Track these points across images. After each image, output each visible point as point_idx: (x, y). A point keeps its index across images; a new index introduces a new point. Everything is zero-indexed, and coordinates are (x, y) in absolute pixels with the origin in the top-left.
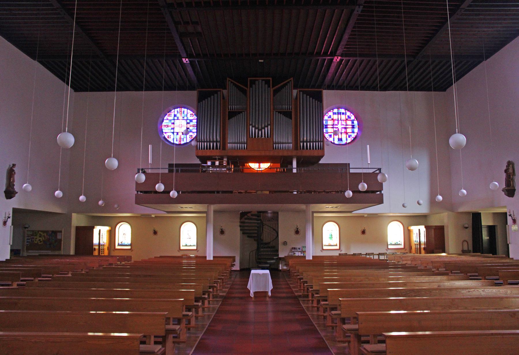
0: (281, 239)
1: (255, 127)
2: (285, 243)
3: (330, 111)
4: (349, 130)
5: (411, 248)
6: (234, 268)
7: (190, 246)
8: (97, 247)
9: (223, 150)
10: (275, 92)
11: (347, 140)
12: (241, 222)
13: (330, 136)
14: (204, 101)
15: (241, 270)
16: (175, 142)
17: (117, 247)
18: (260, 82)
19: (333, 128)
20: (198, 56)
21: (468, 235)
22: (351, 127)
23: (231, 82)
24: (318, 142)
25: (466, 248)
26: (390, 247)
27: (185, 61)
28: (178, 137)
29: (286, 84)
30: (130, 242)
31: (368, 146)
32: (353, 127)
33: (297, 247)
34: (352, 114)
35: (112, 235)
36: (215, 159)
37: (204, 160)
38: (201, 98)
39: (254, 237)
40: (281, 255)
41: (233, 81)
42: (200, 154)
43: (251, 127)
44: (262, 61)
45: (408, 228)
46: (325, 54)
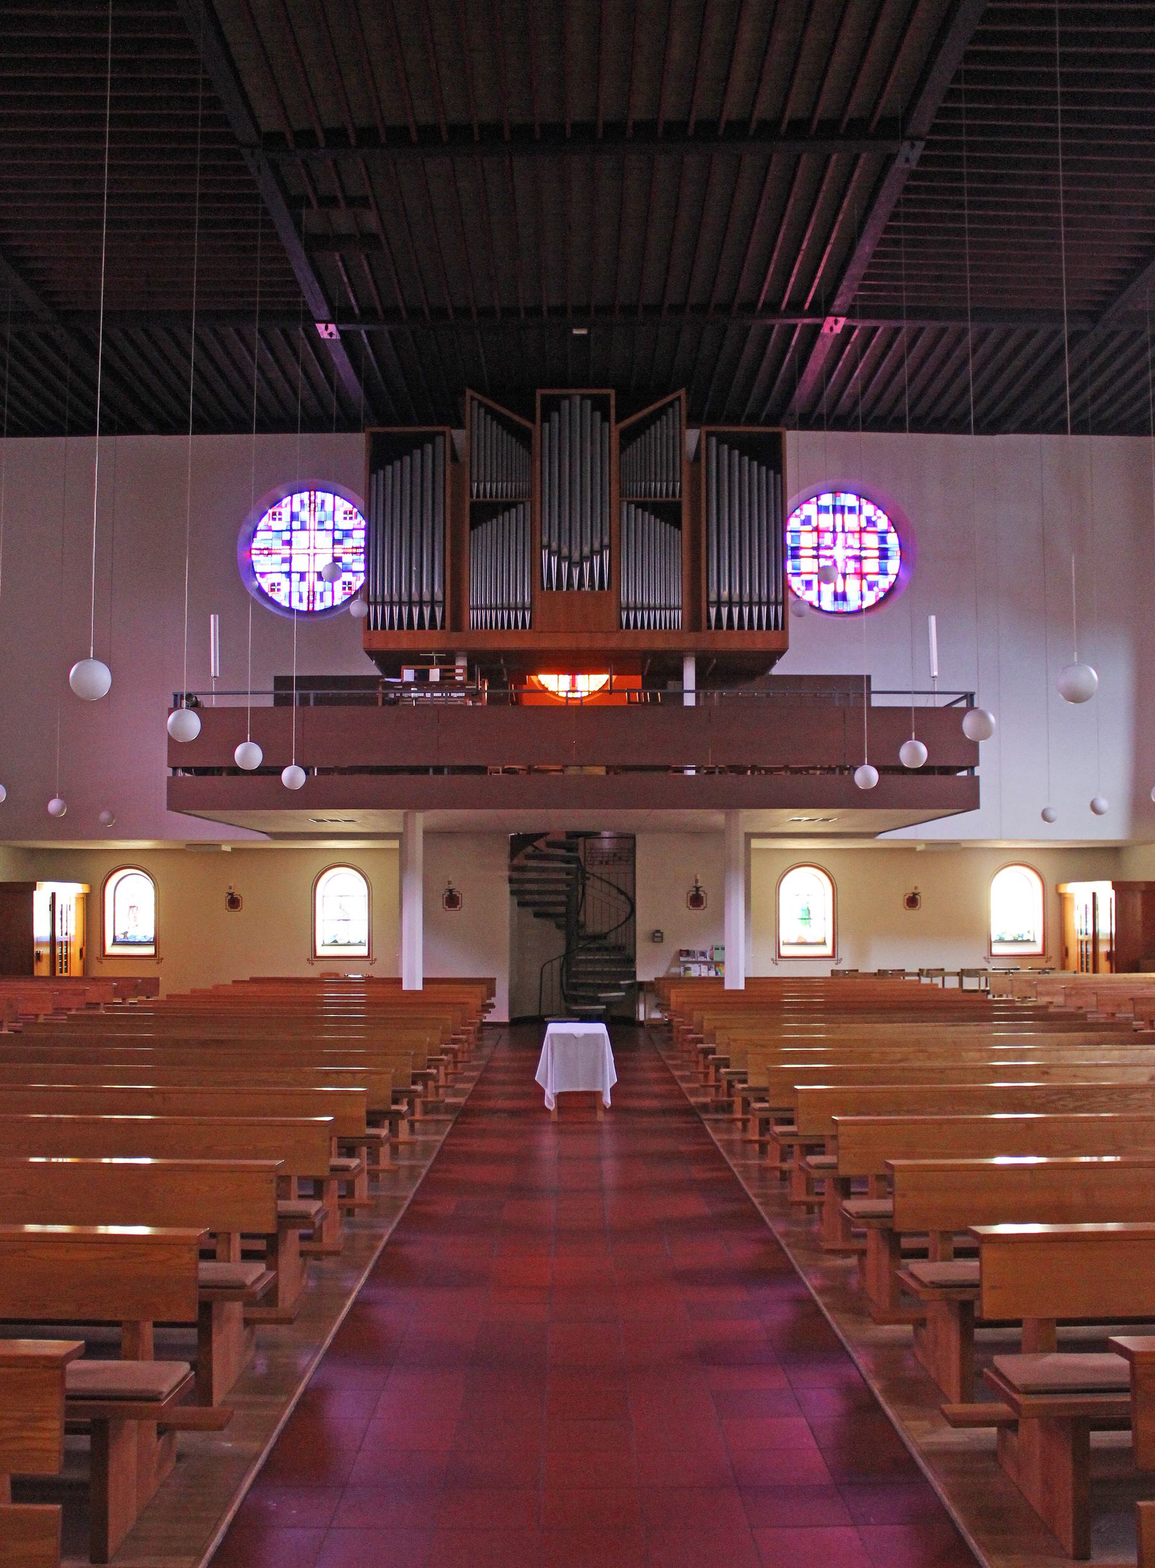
0: (644, 923)
1: (559, 552)
2: (657, 936)
3: (807, 502)
4: (871, 566)
6: (489, 1018)
7: (349, 944)
8: (45, 951)
10: (628, 437)
11: (862, 598)
12: (513, 868)
13: (808, 584)
14: (407, 459)
16: (296, 605)
17: (111, 950)
18: (577, 403)
19: (817, 557)
20: (368, 314)
22: (877, 553)
23: (480, 404)
26: (997, 949)
27: (327, 331)
28: (304, 587)
29: (662, 411)
30: (150, 935)
31: (933, 619)
32: (884, 554)
33: (697, 948)
34: (880, 513)
35: (93, 909)
37: (391, 662)
38: (381, 456)
42: (378, 645)
43: (545, 553)
44: (584, 332)
46: (795, 307)
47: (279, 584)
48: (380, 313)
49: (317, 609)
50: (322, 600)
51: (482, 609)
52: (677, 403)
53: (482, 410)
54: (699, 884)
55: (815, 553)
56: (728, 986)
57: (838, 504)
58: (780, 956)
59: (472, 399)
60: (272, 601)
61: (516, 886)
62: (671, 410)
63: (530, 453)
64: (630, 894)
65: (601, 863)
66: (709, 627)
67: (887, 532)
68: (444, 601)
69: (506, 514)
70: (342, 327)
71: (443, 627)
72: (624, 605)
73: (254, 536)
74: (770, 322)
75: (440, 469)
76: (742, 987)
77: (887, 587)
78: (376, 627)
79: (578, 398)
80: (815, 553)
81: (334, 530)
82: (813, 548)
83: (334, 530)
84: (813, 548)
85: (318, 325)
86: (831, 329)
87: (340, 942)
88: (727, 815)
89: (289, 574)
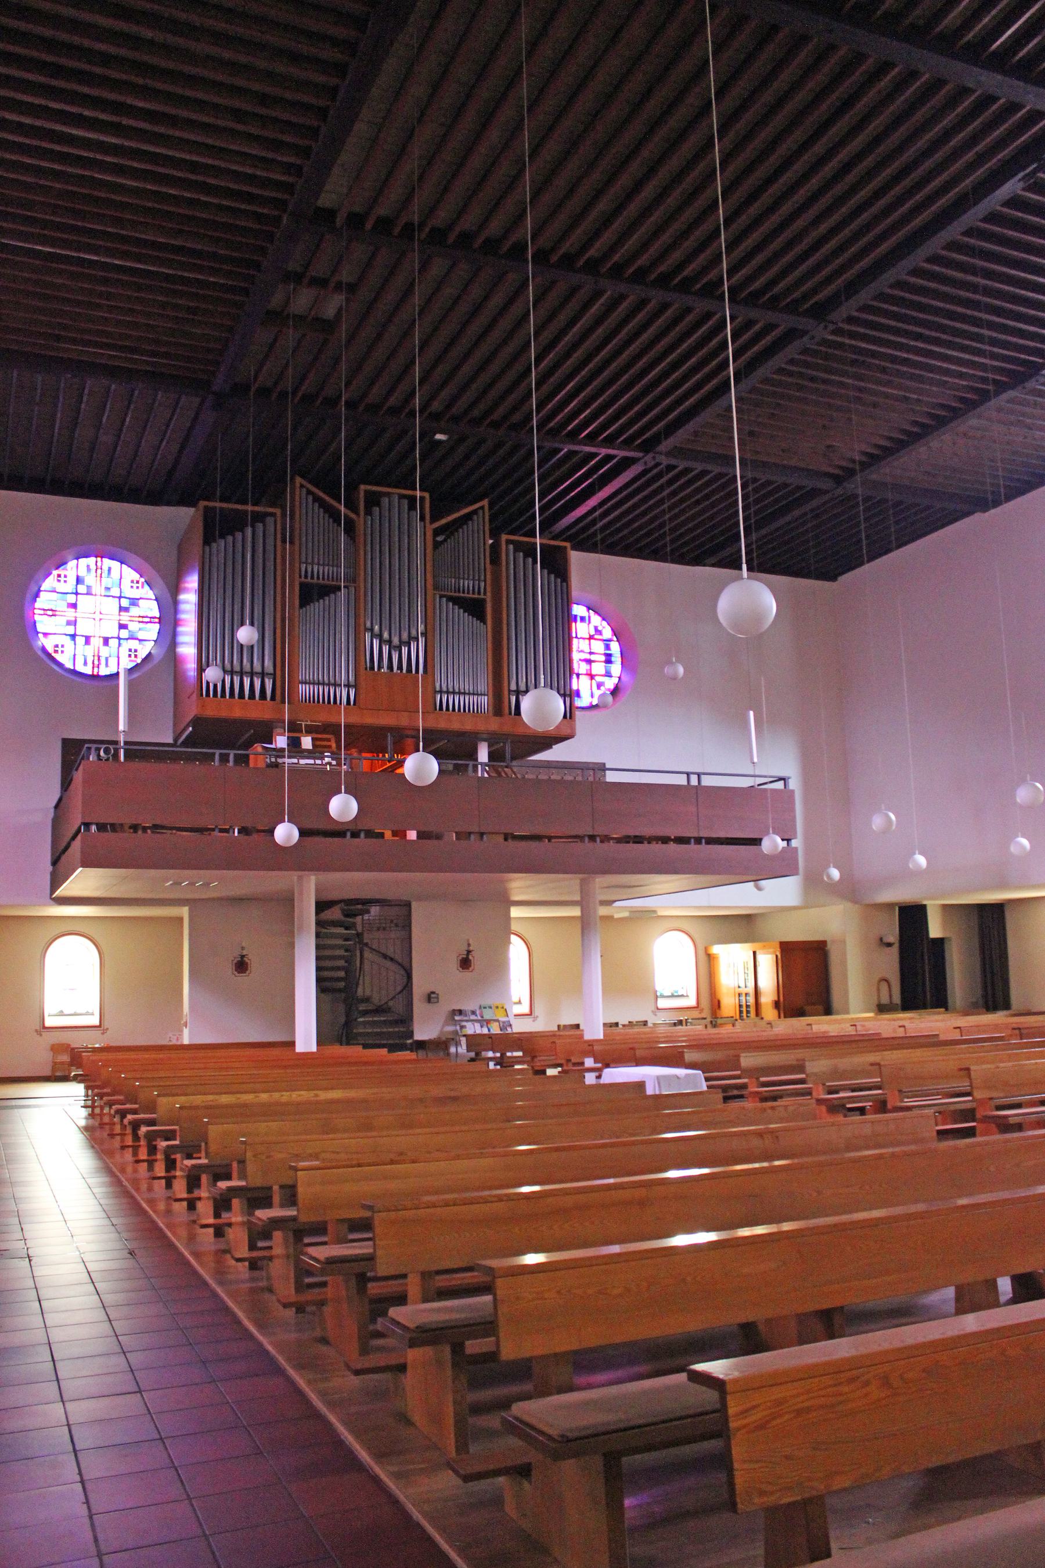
0: (420, 985)
1: (380, 636)
2: (431, 998)
4: (598, 668)
5: (716, 1005)
7: (75, 1014)
14: (249, 531)
16: (80, 668)
21: (889, 963)
22: (603, 658)
23: (309, 492)
25: (885, 1000)
26: (662, 1003)
31: (751, 713)
32: (608, 659)
33: (467, 1007)
34: (604, 623)
38: (216, 528)
43: (368, 635)
45: (706, 949)
50: (107, 665)
51: (310, 683)
52: (481, 512)
53: (310, 498)
54: (471, 948)
59: (302, 486)
62: (475, 517)
66: (510, 713)
67: (610, 640)
68: (274, 674)
73: (37, 595)
77: (612, 687)
78: (208, 694)
81: (120, 598)
83: (120, 598)
87: (66, 1012)
89: (73, 637)
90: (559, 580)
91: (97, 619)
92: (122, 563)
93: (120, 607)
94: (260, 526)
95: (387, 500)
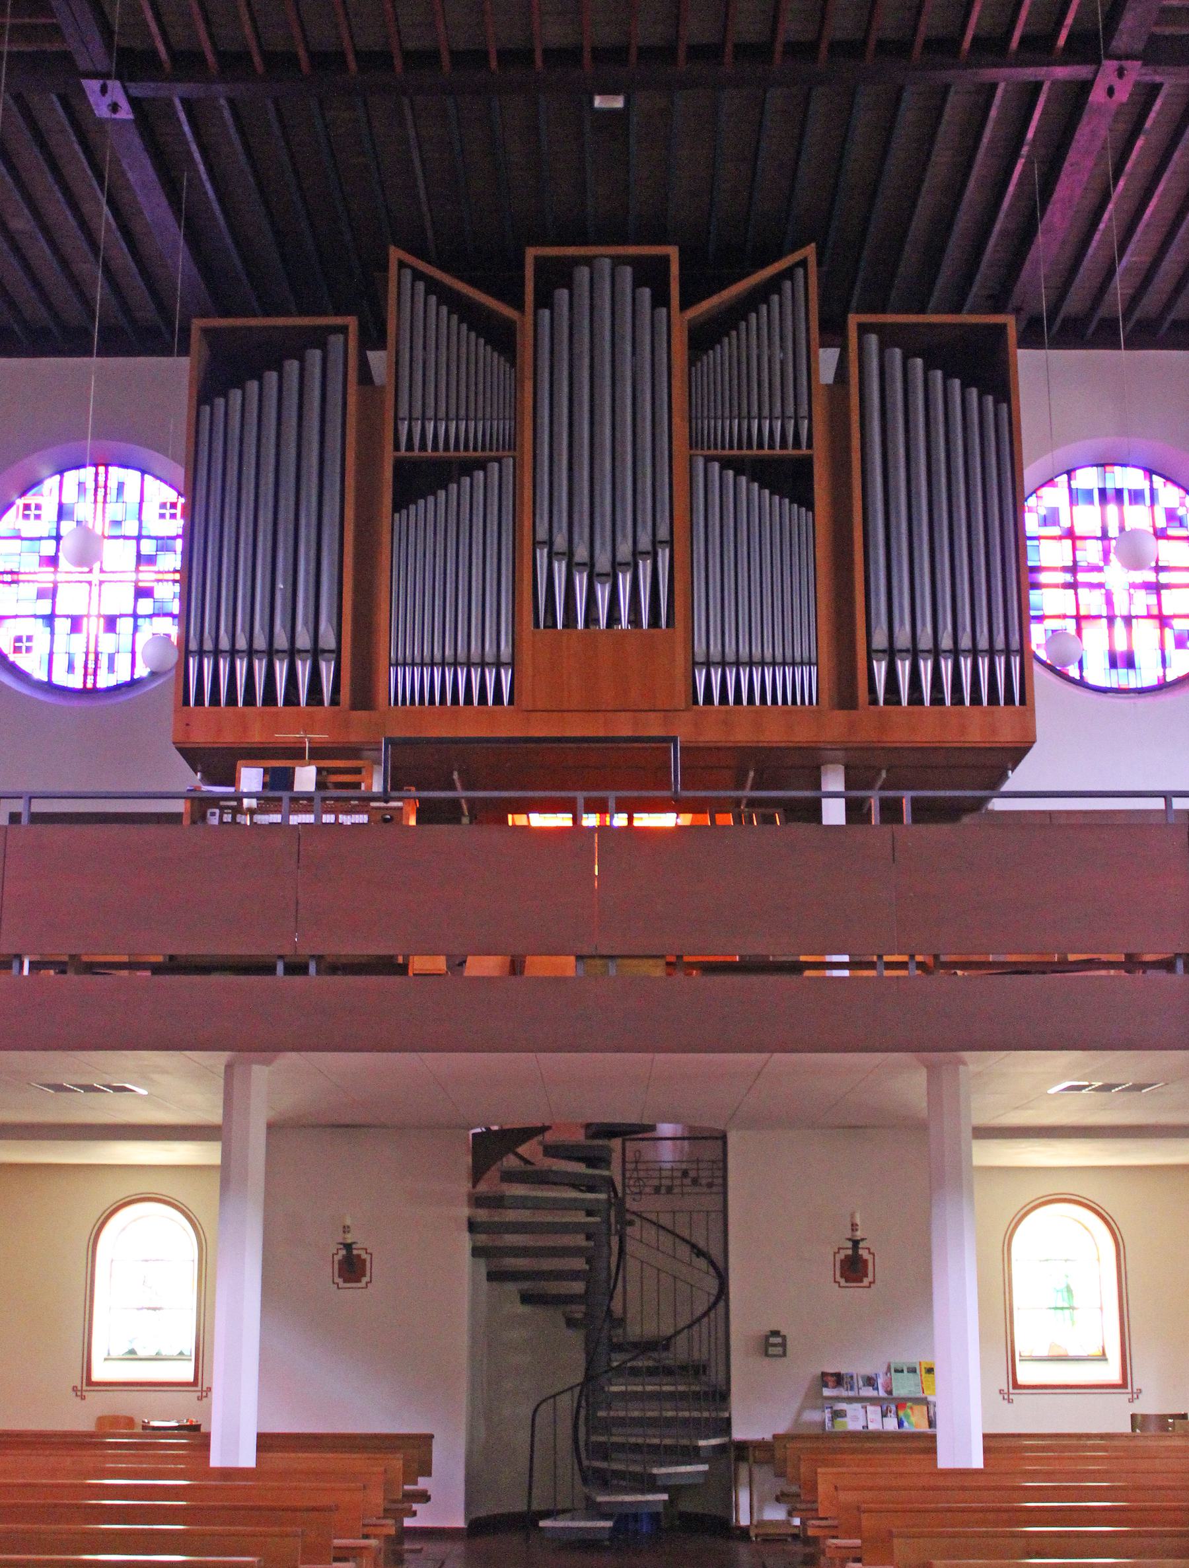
0: (746, 1318)
2: (772, 1344)
3: (1050, 482)
6: (422, 1517)
7: (158, 1358)
9: (354, 707)
10: (703, 338)
12: (478, 1201)
14: (272, 377)
15: (478, 1527)
16: (61, 678)
18: (604, 273)
19: (1074, 586)
20: (188, 62)
23: (418, 275)
24: (992, 653)
27: (108, 101)
28: (79, 641)
29: (773, 285)
33: (858, 1368)
36: (296, 753)
37: (217, 764)
39: (570, 1299)
40: (748, 1426)
41: (422, 266)
42: (201, 737)
43: (542, 555)
44: (618, 103)
46: (1039, 47)
47: (30, 638)
48: (210, 58)
49: (101, 684)
52: (800, 272)
53: (421, 286)
54: (859, 1234)
55: (1068, 578)
56: (945, 1461)
57: (1110, 485)
58: (1016, 1386)
59: (402, 265)
60: (14, 670)
61: (483, 1239)
62: (787, 285)
63: (513, 365)
64: (715, 1251)
65: (657, 1190)
66: (874, 701)
68: (338, 651)
69: (466, 481)
70: (137, 90)
71: (334, 702)
72: (700, 658)
74: (988, 74)
75: (335, 398)
76: (977, 1461)
79: (607, 262)
80: (1068, 578)
81: (139, 538)
82: (1065, 569)
83: (139, 538)
84: (1065, 569)
85: (85, 83)
86: (1111, 92)
87: (141, 1353)
88: (933, 1071)
89: (50, 619)
90: (990, 399)
91: (95, 582)
92: (143, 472)
93: (139, 556)
94: (315, 355)
95: (585, 270)
